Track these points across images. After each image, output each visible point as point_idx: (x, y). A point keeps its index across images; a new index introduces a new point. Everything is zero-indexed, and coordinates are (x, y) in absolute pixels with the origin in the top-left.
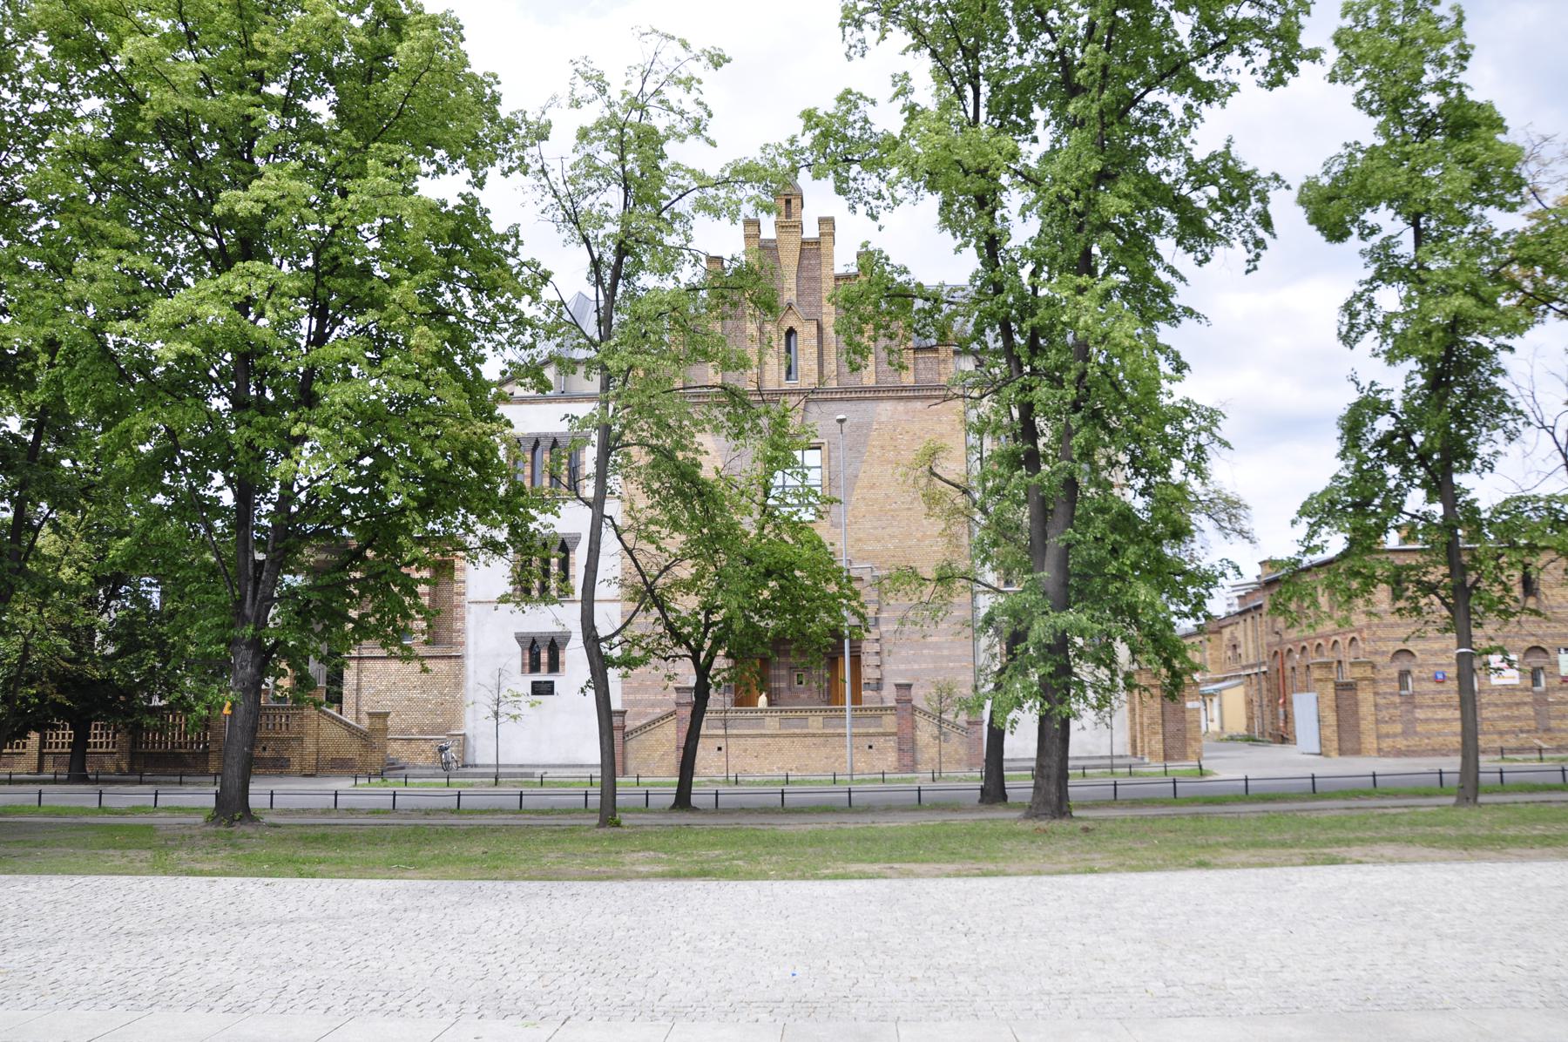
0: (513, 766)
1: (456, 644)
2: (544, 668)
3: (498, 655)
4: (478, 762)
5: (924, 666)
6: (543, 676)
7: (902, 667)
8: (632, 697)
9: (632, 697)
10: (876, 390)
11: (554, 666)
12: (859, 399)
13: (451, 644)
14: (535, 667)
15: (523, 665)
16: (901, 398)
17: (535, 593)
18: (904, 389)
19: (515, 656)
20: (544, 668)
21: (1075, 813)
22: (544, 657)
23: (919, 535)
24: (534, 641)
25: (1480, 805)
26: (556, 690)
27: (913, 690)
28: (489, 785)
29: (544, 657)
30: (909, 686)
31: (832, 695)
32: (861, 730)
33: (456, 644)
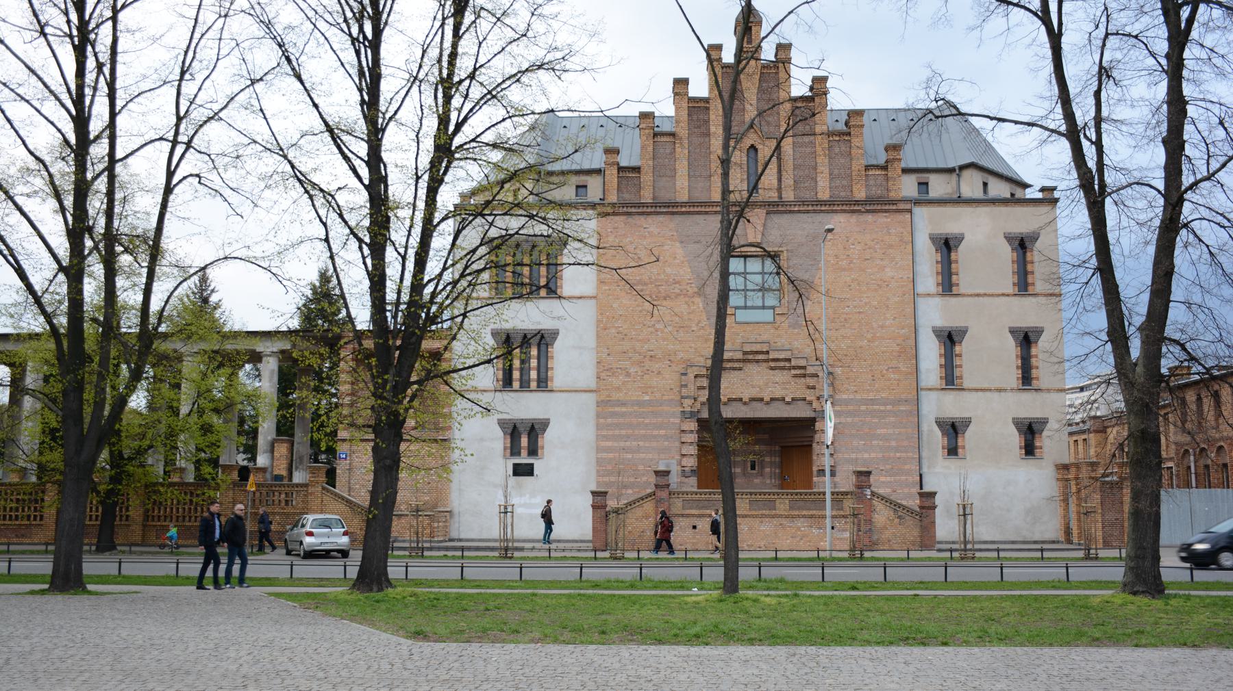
0: (472, 540)
1: (442, 429)
2: (524, 452)
3: (482, 440)
4: (462, 536)
5: (873, 455)
6: (524, 459)
7: (854, 456)
8: (606, 479)
9: (606, 479)
10: (654, 205)
11: (533, 452)
12: (815, 211)
13: (438, 429)
14: (514, 450)
15: (505, 449)
16: (853, 212)
17: (534, 385)
18: (857, 202)
19: (498, 441)
20: (524, 452)
21: (90, 587)
22: (524, 441)
23: (869, 336)
24: (515, 427)
25: (90, 593)
26: (535, 472)
27: (872, 478)
28: (1082, 559)
29: (524, 441)
30: (869, 473)
31: (785, 482)
32: (811, 512)
33: (442, 429)
